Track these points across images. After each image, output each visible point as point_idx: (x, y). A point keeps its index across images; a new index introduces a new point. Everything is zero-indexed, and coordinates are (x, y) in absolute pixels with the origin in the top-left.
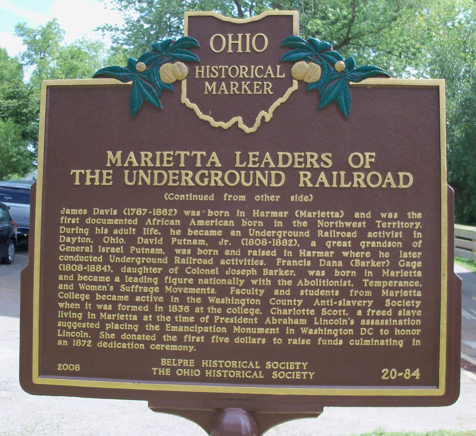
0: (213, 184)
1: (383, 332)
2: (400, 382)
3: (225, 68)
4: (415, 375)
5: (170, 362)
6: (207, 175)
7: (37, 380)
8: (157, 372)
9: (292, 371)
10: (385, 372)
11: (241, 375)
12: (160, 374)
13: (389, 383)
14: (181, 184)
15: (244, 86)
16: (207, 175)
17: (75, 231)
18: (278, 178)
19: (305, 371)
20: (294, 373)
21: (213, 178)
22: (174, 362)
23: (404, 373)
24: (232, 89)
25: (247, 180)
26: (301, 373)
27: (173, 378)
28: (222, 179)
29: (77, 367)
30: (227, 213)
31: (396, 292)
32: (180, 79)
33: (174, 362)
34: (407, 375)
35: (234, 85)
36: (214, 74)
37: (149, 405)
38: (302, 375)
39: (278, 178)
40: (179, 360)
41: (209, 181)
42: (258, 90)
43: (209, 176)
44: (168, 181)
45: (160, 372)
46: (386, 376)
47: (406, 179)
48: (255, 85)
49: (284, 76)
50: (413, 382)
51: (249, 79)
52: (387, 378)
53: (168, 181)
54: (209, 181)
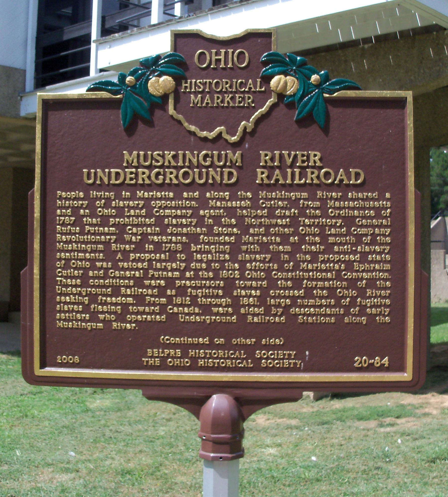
0: (168, 181)
1: (132, 309)
2: (371, 368)
3: (210, 82)
4: (385, 363)
5: (157, 352)
6: (162, 173)
7: (38, 372)
8: (147, 362)
9: (281, 359)
10: (358, 360)
11: (232, 364)
12: (150, 364)
13: (360, 370)
14: (139, 182)
15: (227, 99)
16: (162, 173)
17: (201, 249)
18: (230, 174)
19: (293, 359)
20: (281, 361)
21: (168, 176)
22: (160, 353)
23: (375, 360)
24: (216, 101)
25: (200, 178)
26: (289, 362)
27: (163, 367)
28: (177, 177)
29: (77, 359)
30: (81, 194)
31: (162, 264)
32: (168, 92)
33: (160, 353)
34: (377, 363)
35: (218, 98)
36: (200, 88)
37: (143, 394)
38: (290, 364)
39: (230, 174)
40: (165, 350)
41: (164, 180)
42: (240, 102)
43: (164, 175)
44: (125, 179)
45: (150, 362)
46: (359, 364)
47: (357, 175)
48: (237, 97)
49: (263, 89)
50: (382, 369)
51: (231, 92)
52: (360, 365)
53: (125, 179)
54: (164, 180)
